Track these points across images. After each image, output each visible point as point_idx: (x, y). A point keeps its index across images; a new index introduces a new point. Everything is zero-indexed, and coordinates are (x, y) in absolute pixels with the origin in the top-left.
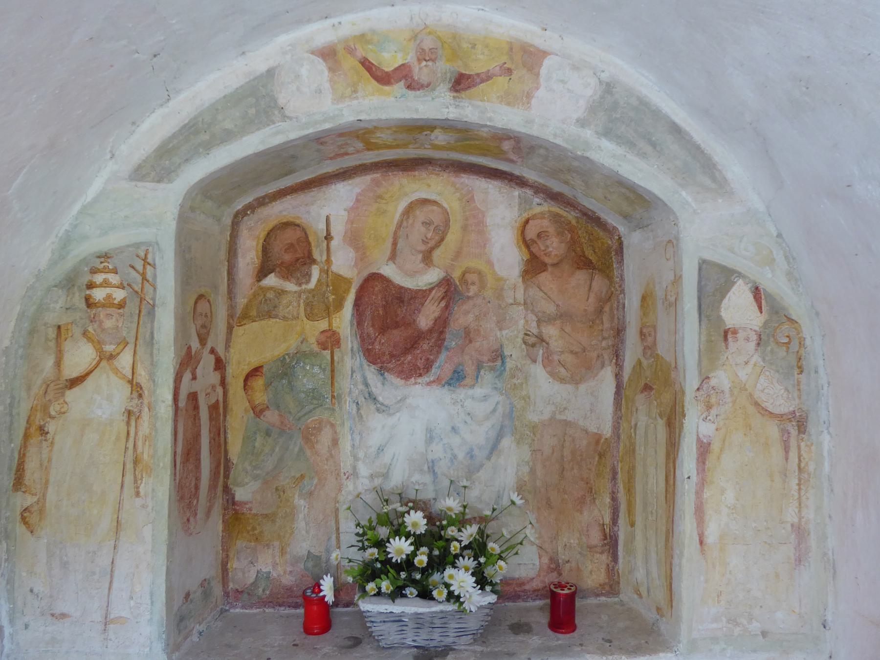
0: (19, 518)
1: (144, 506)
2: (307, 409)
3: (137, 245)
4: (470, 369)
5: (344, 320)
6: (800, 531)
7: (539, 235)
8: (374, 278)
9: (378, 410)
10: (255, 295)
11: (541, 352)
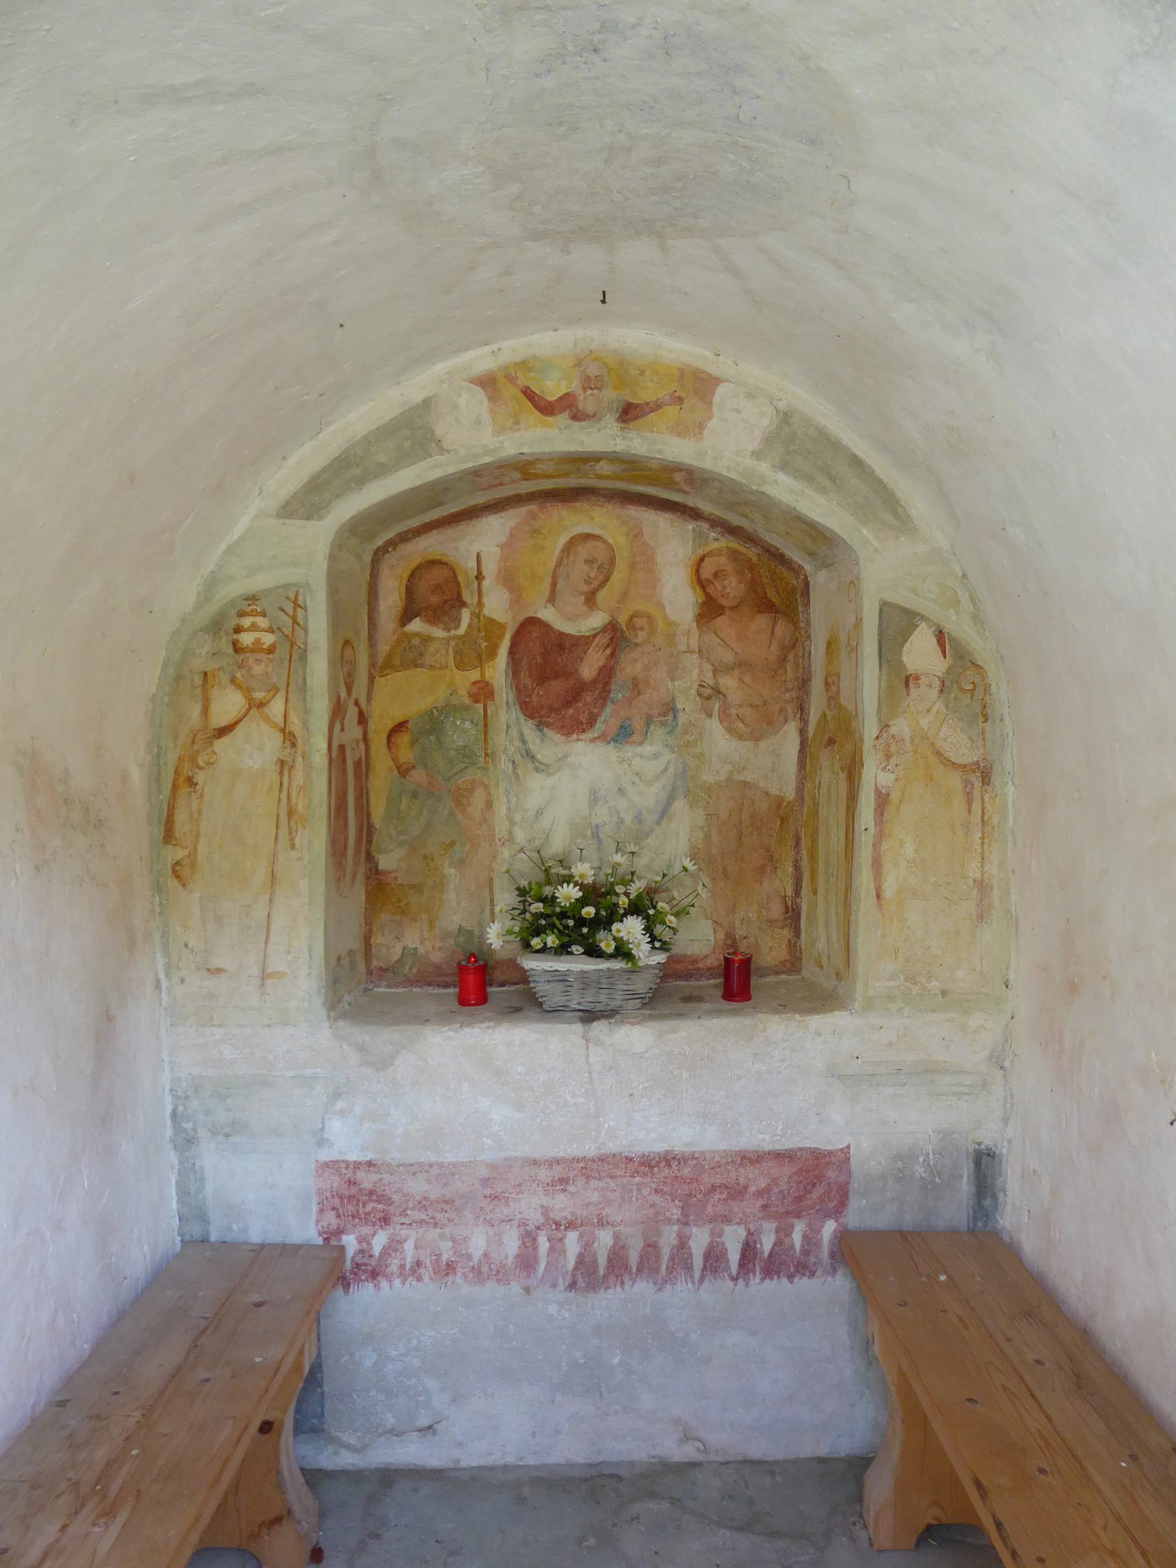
0: (170, 871)
1: (299, 859)
2: (458, 768)
3: (286, 587)
4: (638, 724)
5: (498, 670)
6: (982, 887)
7: (716, 575)
8: (531, 622)
9: (537, 770)
10: (398, 642)
11: (717, 705)
